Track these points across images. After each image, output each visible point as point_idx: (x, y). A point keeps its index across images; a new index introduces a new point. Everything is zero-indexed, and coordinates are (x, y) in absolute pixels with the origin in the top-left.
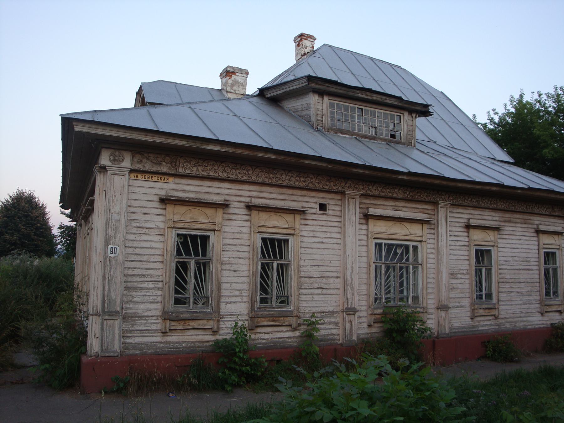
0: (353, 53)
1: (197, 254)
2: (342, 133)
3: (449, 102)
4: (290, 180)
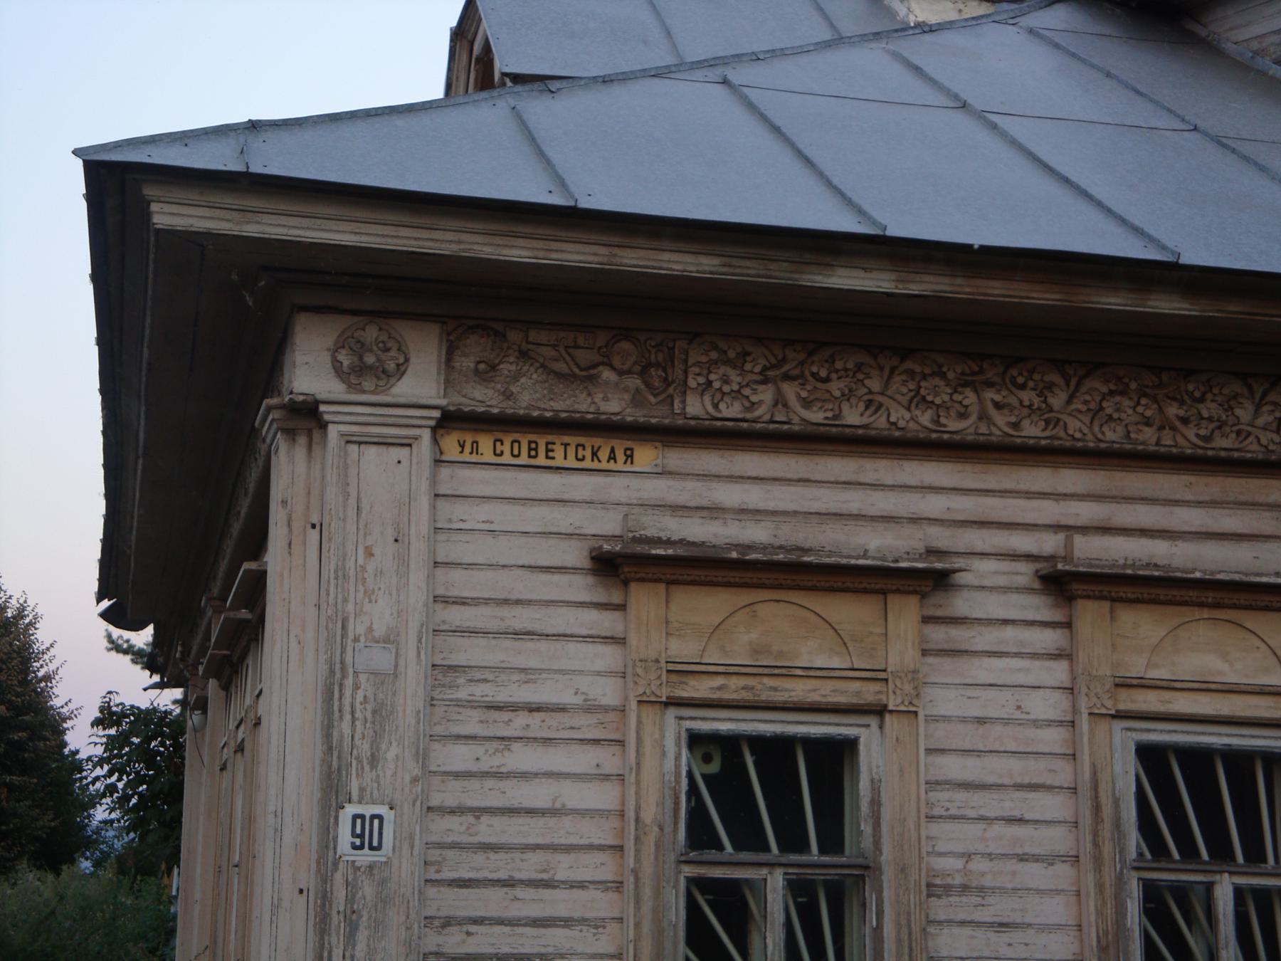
1: (793, 840)
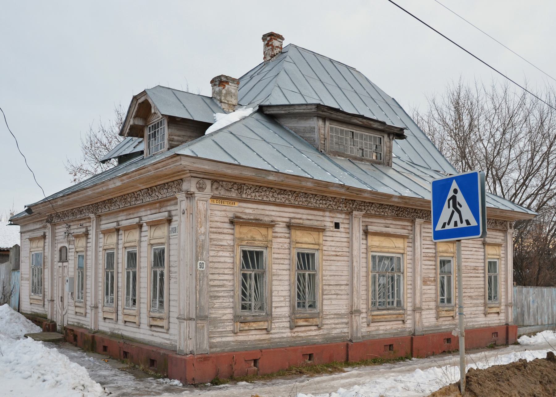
0: (315, 54)
1: (254, 267)
2: (339, 156)
3: (400, 110)
4: (316, 203)
